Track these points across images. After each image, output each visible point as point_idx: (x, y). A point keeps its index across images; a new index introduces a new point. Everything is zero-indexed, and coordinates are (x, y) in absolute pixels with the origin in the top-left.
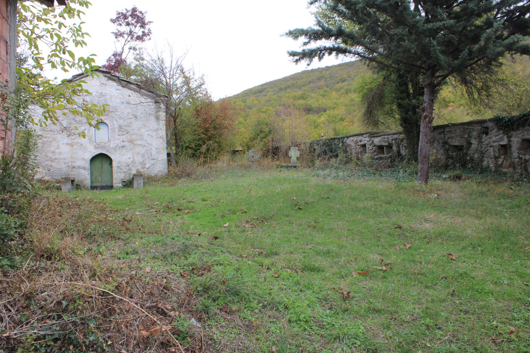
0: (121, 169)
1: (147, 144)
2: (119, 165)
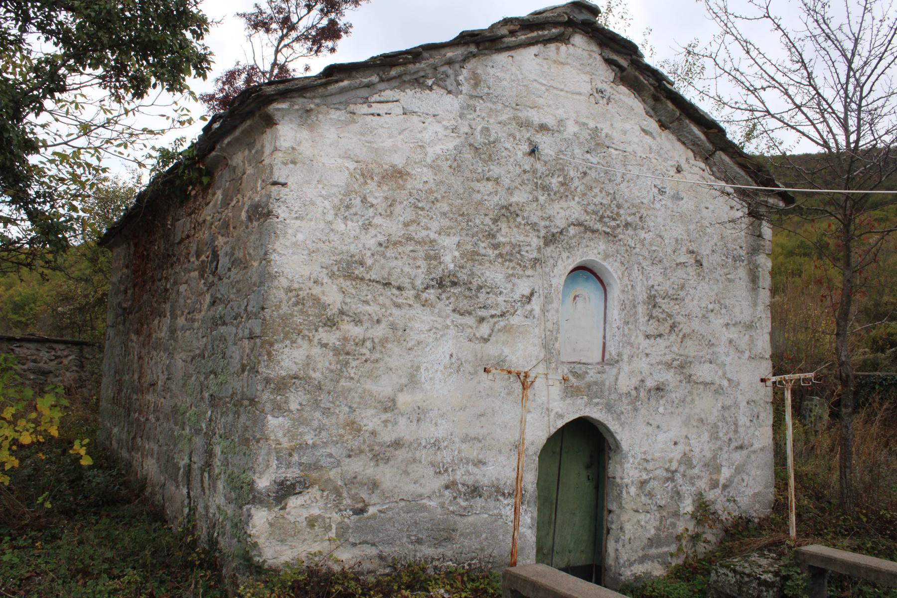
0: (650, 495)
1: (725, 383)
2: (645, 477)
